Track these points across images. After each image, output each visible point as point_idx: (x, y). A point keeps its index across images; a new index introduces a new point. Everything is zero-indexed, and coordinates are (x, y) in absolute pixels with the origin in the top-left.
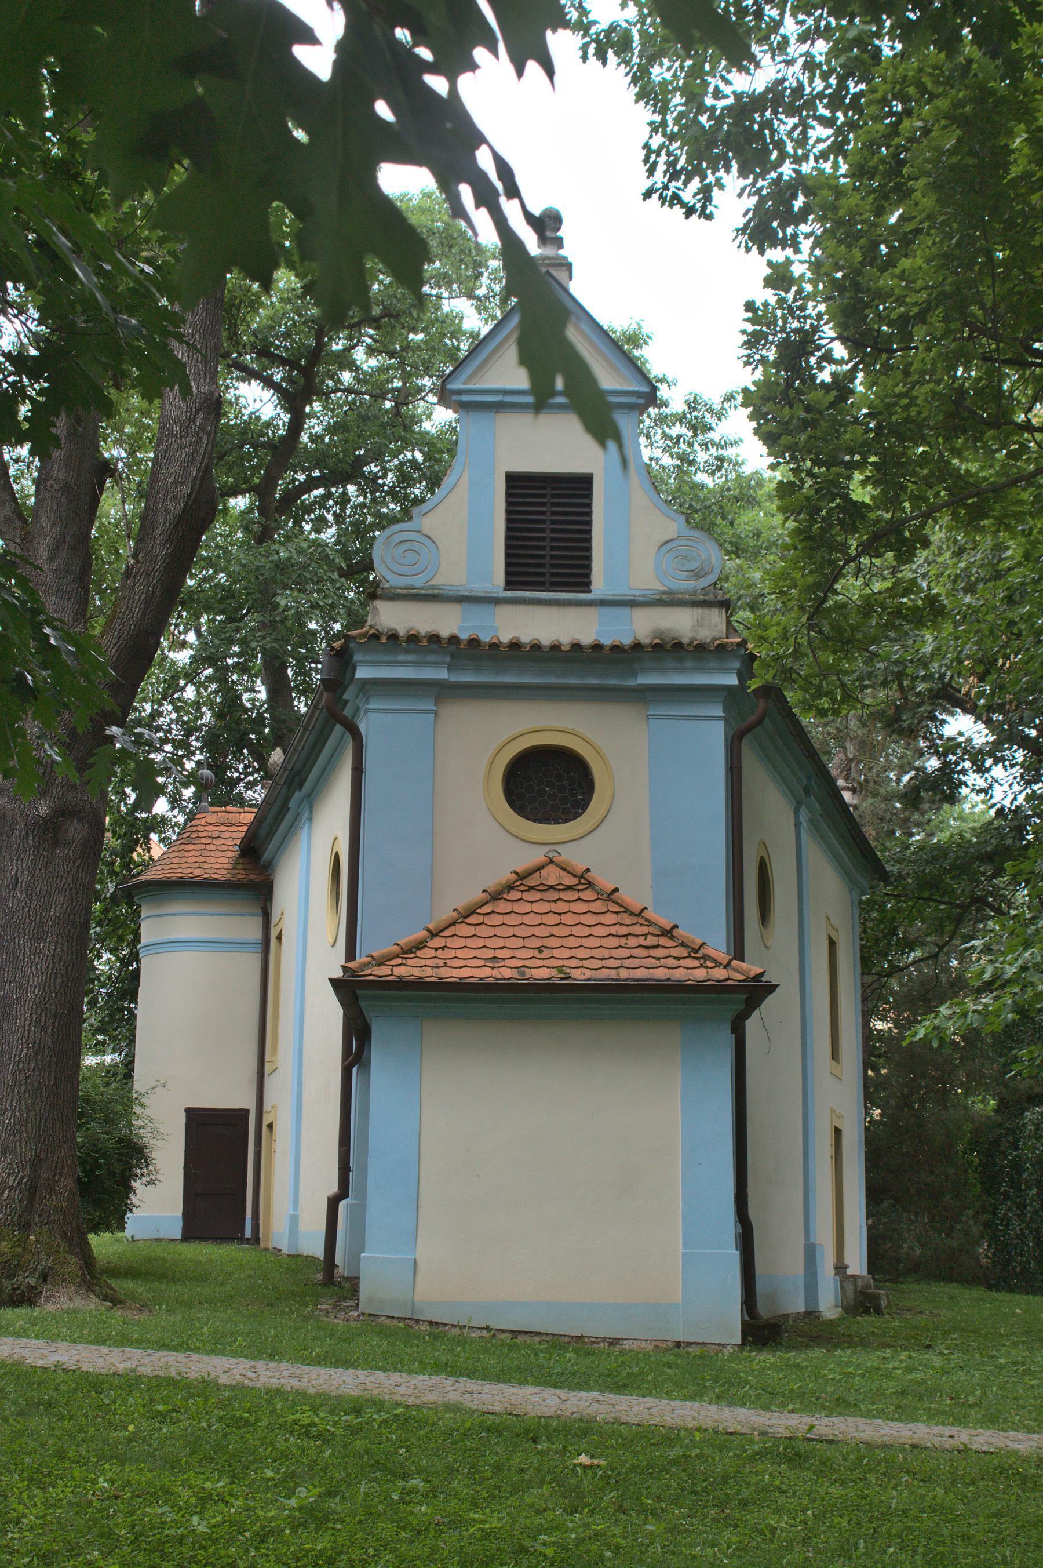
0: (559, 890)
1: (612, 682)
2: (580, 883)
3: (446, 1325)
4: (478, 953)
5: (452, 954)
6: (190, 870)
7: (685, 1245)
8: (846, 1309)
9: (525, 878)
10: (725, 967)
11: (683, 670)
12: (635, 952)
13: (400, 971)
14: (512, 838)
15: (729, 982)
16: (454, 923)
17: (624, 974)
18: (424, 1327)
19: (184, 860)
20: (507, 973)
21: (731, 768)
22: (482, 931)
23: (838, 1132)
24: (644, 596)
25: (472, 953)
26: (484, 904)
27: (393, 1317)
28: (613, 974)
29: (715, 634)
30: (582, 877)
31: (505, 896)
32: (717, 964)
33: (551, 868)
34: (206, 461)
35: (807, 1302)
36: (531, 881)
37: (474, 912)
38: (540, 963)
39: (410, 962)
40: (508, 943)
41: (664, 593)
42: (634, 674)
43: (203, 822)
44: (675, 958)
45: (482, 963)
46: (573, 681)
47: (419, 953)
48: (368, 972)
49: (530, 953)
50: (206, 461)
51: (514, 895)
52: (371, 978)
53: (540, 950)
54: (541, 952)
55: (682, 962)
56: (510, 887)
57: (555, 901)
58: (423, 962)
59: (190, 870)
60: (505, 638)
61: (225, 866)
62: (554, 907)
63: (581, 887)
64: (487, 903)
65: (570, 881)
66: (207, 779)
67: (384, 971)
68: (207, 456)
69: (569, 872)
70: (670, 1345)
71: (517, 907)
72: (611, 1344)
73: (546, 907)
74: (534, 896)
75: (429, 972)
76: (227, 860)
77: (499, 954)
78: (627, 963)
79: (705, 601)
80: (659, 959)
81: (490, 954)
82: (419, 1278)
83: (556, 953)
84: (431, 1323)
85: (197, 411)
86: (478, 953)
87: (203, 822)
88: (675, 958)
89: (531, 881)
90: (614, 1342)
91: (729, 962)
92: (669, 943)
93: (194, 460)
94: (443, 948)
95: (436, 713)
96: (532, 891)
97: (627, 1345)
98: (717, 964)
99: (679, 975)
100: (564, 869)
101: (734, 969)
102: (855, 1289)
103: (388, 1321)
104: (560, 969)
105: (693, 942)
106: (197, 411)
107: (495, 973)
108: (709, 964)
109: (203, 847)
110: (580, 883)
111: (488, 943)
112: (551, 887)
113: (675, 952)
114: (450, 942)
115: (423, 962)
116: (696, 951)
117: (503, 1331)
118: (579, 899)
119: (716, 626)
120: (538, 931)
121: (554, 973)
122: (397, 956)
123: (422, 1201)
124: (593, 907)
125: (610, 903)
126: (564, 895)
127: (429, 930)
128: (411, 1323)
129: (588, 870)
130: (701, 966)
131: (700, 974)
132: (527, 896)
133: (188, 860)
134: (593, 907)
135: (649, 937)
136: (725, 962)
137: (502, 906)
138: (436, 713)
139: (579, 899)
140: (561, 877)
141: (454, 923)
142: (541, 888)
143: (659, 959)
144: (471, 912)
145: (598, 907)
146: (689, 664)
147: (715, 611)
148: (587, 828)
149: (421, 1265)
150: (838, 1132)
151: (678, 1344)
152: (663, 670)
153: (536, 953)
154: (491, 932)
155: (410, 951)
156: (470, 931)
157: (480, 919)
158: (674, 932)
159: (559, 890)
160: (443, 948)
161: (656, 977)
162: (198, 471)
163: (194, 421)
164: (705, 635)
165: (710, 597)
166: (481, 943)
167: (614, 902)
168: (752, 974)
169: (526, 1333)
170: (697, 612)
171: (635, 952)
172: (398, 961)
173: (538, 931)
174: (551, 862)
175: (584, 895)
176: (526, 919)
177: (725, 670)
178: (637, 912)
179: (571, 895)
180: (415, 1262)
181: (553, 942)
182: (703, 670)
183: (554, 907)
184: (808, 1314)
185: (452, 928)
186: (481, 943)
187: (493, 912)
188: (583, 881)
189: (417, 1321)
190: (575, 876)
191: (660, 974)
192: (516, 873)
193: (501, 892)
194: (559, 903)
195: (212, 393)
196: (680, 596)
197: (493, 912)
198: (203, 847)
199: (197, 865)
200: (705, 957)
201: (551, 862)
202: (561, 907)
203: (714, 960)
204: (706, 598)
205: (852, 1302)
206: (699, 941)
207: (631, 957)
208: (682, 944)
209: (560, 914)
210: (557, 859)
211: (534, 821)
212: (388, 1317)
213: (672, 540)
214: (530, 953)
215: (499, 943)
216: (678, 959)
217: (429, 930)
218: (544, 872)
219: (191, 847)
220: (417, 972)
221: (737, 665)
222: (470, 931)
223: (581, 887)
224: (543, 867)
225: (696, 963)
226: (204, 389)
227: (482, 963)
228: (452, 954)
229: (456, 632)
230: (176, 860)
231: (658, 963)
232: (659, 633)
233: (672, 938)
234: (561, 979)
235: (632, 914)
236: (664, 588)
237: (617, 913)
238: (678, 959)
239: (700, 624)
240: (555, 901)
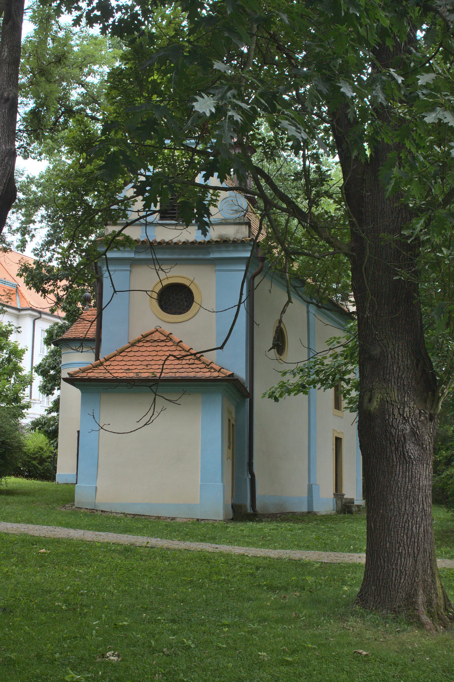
0: (159, 342)
1: (200, 257)
2: (167, 339)
3: (108, 512)
4: (122, 367)
5: (112, 367)
6: (78, 334)
7: (201, 481)
8: (337, 511)
9: (146, 337)
10: (218, 372)
11: (228, 251)
12: (184, 366)
13: (90, 375)
14: (159, 320)
15: (219, 378)
16: (115, 356)
17: (178, 375)
18: (100, 513)
19: (77, 330)
20: (131, 375)
21: (250, 291)
22: (126, 358)
23: (338, 441)
24: (215, 221)
25: (120, 367)
26: (128, 348)
27: (87, 509)
28: (173, 375)
29: (244, 236)
30: (168, 336)
31: (137, 345)
32: (215, 370)
33: (157, 333)
34: (9, 176)
35: (308, 508)
36: (148, 339)
37: (124, 351)
38: (146, 371)
39: (95, 371)
40: (135, 363)
41: (223, 220)
42: (209, 253)
43: (86, 314)
44: (199, 368)
45: (123, 371)
46: (184, 257)
47: (100, 368)
48: (78, 375)
49: (143, 367)
50: (9, 176)
51: (141, 344)
52: (78, 377)
53: (147, 365)
54: (147, 366)
55: (202, 370)
56: (139, 341)
57: (156, 346)
58: (100, 371)
59: (78, 334)
60: (158, 240)
61: (93, 332)
62: (156, 349)
63: (167, 340)
64: (129, 347)
65: (163, 338)
66: (88, 297)
67: (85, 374)
68: (10, 174)
69: (163, 335)
70: (195, 520)
71: (141, 349)
72: (172, 520)
73: (152, 349)
74: (149, 344)
75: (102, 374)
76: (94, 330)
77: (131, 367)
78: (180, 370)
79: (239, 223)
80: (193, 369)
81: (127, 367)
82: (97, 494)
83: (153, 367)
84: (102, 511)
85: (5, 156)
86: (122, 367)
87: (86, 314)
88: (199, 368)
89: (148, 339)
90: (173, 519)
91: (220, 370)
92: (199, 362)
93: (4, 176)
94: (109, 365)
95: (130, 271)
96: (148, 343)
97: (178, 520)
98: (215, 370)
99: (199, 375)
100: (162, 334)
101: (222, 373)
102: (342, 504)
103: (86, 510)
104: (153, 373)
105: (207, 362)
106: (5, 156)
107: (127, 375)
108: (212, 370)
109: (85, 324)
110: (167, 339)
111: (127, 363)
112: (155, 341)
113: (200, 366)
114: (113, 363)
115: (100, 371)
116: (208, 365)
117: (130, 514)
118: (166, 345)
119: (244, 233)
120: (148, 358)
121: (150, 375)
122: (91, 369)
123: (99, 464)
124: (171, 348)
125: (178, 347)
126: (160, 344)
127: (105, 358)
128: (94, 511)
129: (171, 334)
130: (209, 371)
131: (208, 375)
132: (145, 344)
133: (79, 330)
134: (171, 348)
135: (191, 360)
136: (218, 370)
137: (135, 349)
138: (130, 271)
139: (166, 345)
140: (160, 337)
141: (115, 356)
142: (151, 341)
143: (193, 369)
144: (123, 351)
145: (173, 348)
146: (231, 249)
147: (244, 227)
148: (190, 316)
149: (98, 489)
150: (338, 441)
151: (198, 520)
152: (220, 252)
153: (145, 367)
154: (130, 358)
155: (96, 367)
156: (121, 358)
157: (125, 354)
158: (201, 358)
159: (159, 342)
160: (109, 365)
161: (190, 376)
162: (6, 180)
163: (4, 160)
164: (240, 236)
165: (242, 221)
166: (124, 363)
167: (179, 346)
168: (228, 374)
169: (139, 515)
170: (237, 227)
171: (184, 366)
172: (91, 371)
173: (148, 358)
174: (157, 330)
175: (168, 344)
176: (144, 354)
177: (246, 251)
178: (187, 350)
179: (163, 344)
180: (96, 487)
181: (153, 363)
182: (237, 251)
183: (156, 349)
184: (309, 513)
185: (115, 357)
186: (124, 363)
187: (131, 351)
188: (168, 338)
189: (97, 510)
190: (165, 336)
191: (192, 375)
192: (142, 335)
193: (135, 343)
194: (158, 347)
195: (12, 149)
196: (229, 221)
197: (131, 351)
198: (85, 324)
199: (82, 332)
200: (211, 368)
201: (157, 330)
202: (158, 348)
203: (214, 369)
204: (240, 221)
205: (340, 509)
206: (210, 361)
207: (182, 368)
208: (203, 363)
209: (157, 351)
210: (159, 330)
211: (171, 314)
212: (86, 509)
213: (227, 198)
214: (143, 367)
215: (132, 363)
216: (201, 368)
217: (105, 358)
218: (153, 335)
219: (80, 325)
220: (97, 375)
221: (251, 248)
222: (121, 358)
223: (167, 340)
224: (153, 333)
225: (207, 370)
226: (8, 147)
227: (123, 371)
228: (112, 367)
229: (139, 238)
230: (74, 330)
231: (192, 370)
232: (221, 237)
233: (200, 360)
234: (152, 377)
235: (186, 351)
236: (223, 218)
237: (180, 351)
238: (201, 368)
239: (237, 232)
240: (156, 346)
